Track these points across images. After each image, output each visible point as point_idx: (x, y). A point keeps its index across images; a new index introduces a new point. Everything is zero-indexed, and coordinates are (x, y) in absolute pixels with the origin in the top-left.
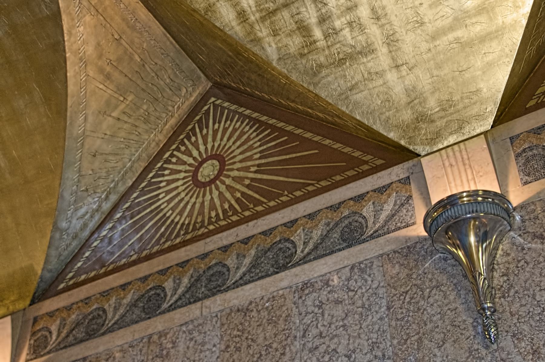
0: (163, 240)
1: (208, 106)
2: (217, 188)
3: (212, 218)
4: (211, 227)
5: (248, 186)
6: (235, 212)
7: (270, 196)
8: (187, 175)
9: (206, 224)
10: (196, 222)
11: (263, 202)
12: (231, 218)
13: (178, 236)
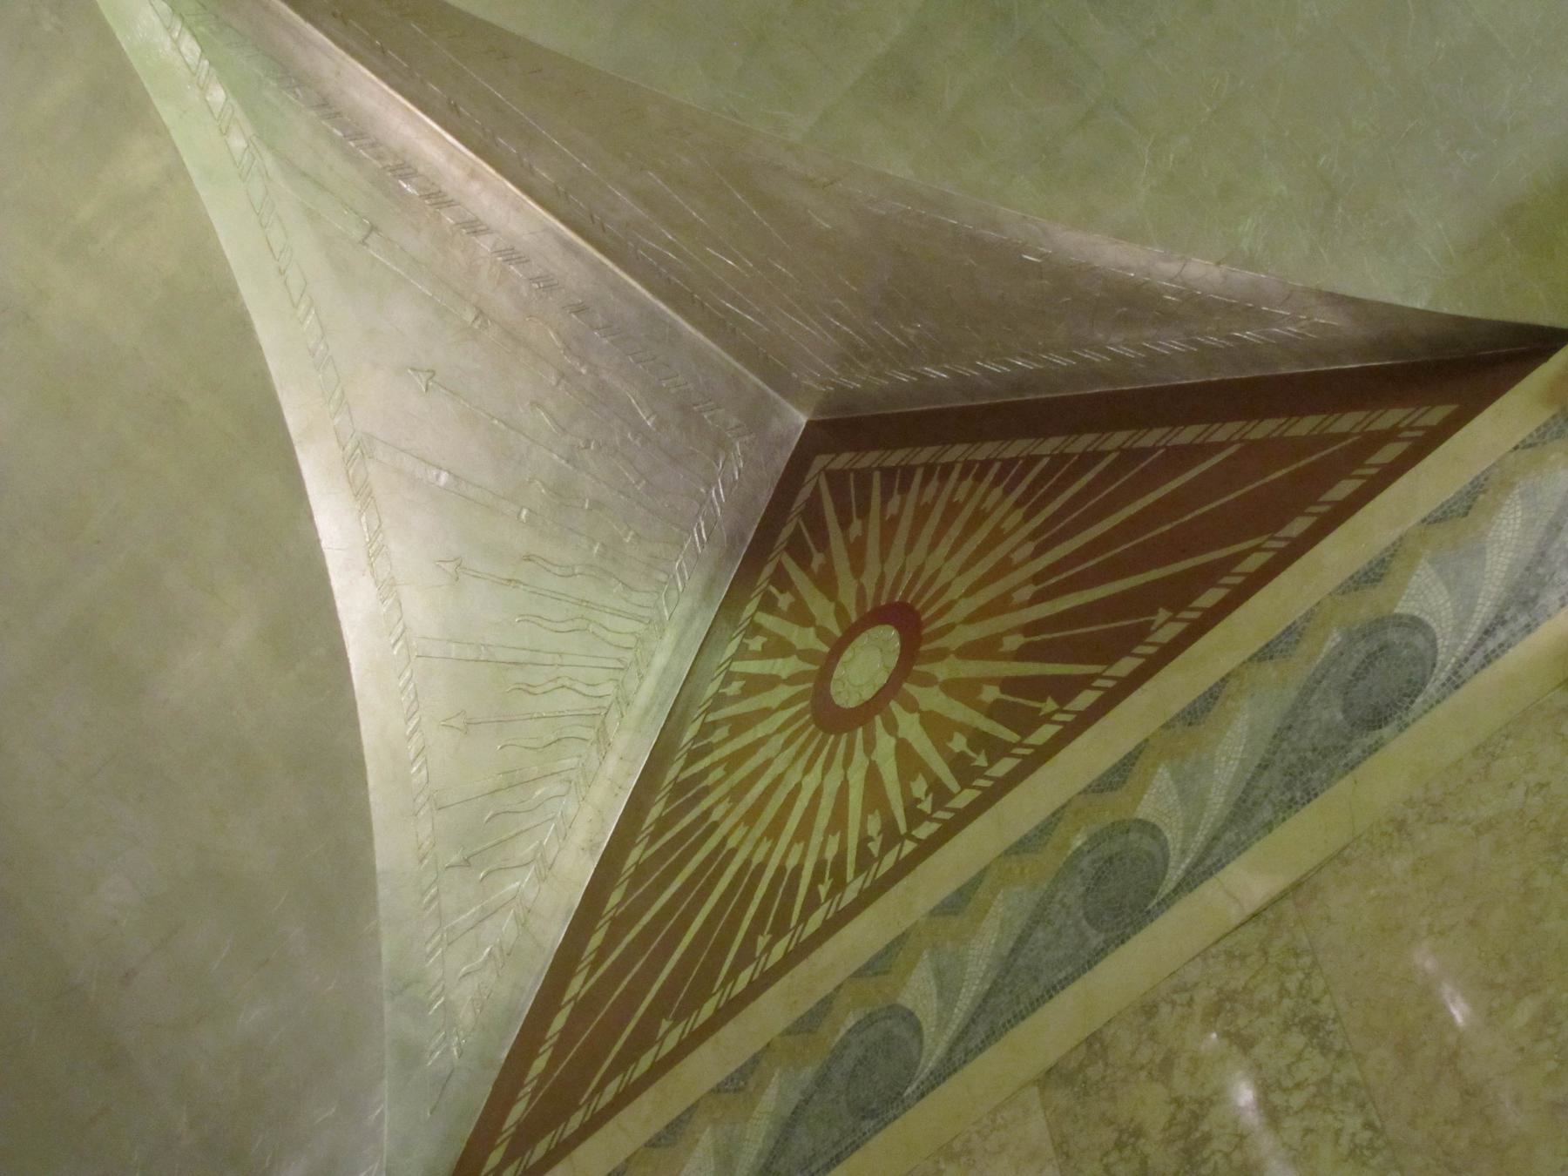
0: (762, 941)
1: (813, 483)
2: (891, 727)
3: (918, 801)
4: (925, 831)
5: (1021, 655)
6: (997, 750)
7: (1107, 650)
8: (940, 623)
9: (903, 828)
10: (864, 840)
11: (1093, 677)
12: (987, 773)
13: (812, 903)
